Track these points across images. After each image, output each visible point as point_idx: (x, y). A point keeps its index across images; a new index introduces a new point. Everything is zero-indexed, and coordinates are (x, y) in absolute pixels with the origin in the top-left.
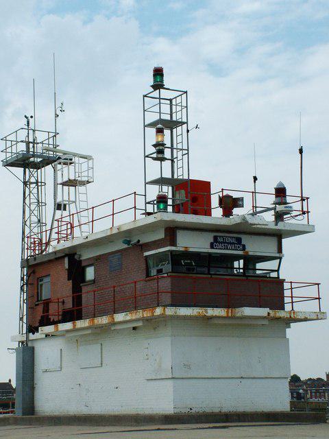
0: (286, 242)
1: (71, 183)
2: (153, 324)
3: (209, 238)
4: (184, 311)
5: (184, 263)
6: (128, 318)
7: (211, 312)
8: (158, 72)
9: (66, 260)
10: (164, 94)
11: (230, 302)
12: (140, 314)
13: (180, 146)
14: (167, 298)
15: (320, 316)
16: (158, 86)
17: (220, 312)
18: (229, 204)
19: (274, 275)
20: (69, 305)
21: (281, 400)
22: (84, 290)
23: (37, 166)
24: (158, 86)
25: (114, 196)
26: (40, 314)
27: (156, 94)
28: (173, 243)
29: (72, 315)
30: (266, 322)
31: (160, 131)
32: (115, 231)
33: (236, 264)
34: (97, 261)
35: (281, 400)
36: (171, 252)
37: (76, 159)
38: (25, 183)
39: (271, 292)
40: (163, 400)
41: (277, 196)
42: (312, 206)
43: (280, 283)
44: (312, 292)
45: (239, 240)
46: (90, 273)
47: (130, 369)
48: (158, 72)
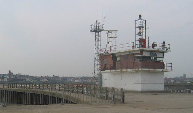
0: (164, 53)
1: (112, 37)
2: (137, 72)
3: (149, 53)
4: (146, 69)
5: (146, 59)
6: (132, 70)
7: (151, 70)
8: (140, 16)
9: (112, 55)
10: (141, 20)
11: (154, 67)
12: (135, 70)
13: (143, 32)
14: (141, 67)
15: (172, 70)
16: (140, 19)
17: (152, 70)
18: (154, 45)
19: (162, 61)
20: (112, 65)
21: (161, 88)
22: (117, 63)
23: (98, 32)
24: (140, 19)
25: (125, 42)
26: (104, 68)
27: (139, 20)
28: (142, 54)
29: (111, 68)
30: (161, 72)
31: (140, 29)
32: (128, 50)
33: (151, 58)
34: (120, 56)
35: (161, 88)
36: (142, 56)
37: (112, 32)
38: (95, 36)
39: (161, 65)
40: (139, 88)
41: (163, 44)
42: (104, 26)
43: (163, 63)
44: (170, 65)
45: (155, 54)
46: (118, 59)
47: (130, 81)
48: (140, 16)
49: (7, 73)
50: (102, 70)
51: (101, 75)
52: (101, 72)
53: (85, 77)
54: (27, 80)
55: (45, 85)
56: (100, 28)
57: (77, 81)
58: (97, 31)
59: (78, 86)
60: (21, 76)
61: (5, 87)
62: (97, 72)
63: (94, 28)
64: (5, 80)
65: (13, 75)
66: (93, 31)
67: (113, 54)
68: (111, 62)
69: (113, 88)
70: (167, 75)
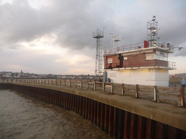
10: (154, 22)
20: (119, 64)
22: (124, 62)
46: (125, 58)
49: (20, 72)
50: (107, 69)
51: (106, 73)
52: (106, 70)
53: (48, 75)
54: (33, 77)
55: (63, 81)
56: (101, 35)
57: (63, 77)
58: (98, 37)
59: (96, 83)
60: (28, 74)
61: (18, 82)
62: (103, 70)
63: (96, 35)
64: (18, 76)
65: (24, 74)
66: (95, 37)
67: (120, 55)
68: (118, 62)
69: (137, 85)
70: (171, 73)
